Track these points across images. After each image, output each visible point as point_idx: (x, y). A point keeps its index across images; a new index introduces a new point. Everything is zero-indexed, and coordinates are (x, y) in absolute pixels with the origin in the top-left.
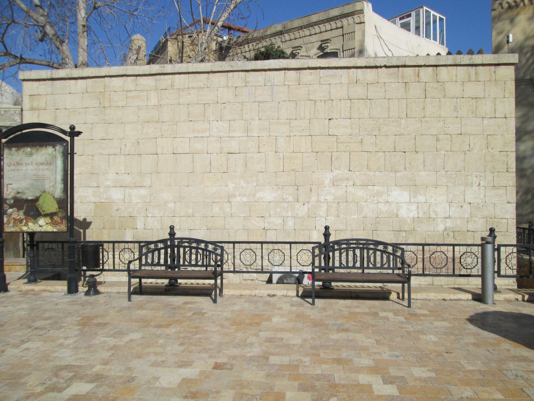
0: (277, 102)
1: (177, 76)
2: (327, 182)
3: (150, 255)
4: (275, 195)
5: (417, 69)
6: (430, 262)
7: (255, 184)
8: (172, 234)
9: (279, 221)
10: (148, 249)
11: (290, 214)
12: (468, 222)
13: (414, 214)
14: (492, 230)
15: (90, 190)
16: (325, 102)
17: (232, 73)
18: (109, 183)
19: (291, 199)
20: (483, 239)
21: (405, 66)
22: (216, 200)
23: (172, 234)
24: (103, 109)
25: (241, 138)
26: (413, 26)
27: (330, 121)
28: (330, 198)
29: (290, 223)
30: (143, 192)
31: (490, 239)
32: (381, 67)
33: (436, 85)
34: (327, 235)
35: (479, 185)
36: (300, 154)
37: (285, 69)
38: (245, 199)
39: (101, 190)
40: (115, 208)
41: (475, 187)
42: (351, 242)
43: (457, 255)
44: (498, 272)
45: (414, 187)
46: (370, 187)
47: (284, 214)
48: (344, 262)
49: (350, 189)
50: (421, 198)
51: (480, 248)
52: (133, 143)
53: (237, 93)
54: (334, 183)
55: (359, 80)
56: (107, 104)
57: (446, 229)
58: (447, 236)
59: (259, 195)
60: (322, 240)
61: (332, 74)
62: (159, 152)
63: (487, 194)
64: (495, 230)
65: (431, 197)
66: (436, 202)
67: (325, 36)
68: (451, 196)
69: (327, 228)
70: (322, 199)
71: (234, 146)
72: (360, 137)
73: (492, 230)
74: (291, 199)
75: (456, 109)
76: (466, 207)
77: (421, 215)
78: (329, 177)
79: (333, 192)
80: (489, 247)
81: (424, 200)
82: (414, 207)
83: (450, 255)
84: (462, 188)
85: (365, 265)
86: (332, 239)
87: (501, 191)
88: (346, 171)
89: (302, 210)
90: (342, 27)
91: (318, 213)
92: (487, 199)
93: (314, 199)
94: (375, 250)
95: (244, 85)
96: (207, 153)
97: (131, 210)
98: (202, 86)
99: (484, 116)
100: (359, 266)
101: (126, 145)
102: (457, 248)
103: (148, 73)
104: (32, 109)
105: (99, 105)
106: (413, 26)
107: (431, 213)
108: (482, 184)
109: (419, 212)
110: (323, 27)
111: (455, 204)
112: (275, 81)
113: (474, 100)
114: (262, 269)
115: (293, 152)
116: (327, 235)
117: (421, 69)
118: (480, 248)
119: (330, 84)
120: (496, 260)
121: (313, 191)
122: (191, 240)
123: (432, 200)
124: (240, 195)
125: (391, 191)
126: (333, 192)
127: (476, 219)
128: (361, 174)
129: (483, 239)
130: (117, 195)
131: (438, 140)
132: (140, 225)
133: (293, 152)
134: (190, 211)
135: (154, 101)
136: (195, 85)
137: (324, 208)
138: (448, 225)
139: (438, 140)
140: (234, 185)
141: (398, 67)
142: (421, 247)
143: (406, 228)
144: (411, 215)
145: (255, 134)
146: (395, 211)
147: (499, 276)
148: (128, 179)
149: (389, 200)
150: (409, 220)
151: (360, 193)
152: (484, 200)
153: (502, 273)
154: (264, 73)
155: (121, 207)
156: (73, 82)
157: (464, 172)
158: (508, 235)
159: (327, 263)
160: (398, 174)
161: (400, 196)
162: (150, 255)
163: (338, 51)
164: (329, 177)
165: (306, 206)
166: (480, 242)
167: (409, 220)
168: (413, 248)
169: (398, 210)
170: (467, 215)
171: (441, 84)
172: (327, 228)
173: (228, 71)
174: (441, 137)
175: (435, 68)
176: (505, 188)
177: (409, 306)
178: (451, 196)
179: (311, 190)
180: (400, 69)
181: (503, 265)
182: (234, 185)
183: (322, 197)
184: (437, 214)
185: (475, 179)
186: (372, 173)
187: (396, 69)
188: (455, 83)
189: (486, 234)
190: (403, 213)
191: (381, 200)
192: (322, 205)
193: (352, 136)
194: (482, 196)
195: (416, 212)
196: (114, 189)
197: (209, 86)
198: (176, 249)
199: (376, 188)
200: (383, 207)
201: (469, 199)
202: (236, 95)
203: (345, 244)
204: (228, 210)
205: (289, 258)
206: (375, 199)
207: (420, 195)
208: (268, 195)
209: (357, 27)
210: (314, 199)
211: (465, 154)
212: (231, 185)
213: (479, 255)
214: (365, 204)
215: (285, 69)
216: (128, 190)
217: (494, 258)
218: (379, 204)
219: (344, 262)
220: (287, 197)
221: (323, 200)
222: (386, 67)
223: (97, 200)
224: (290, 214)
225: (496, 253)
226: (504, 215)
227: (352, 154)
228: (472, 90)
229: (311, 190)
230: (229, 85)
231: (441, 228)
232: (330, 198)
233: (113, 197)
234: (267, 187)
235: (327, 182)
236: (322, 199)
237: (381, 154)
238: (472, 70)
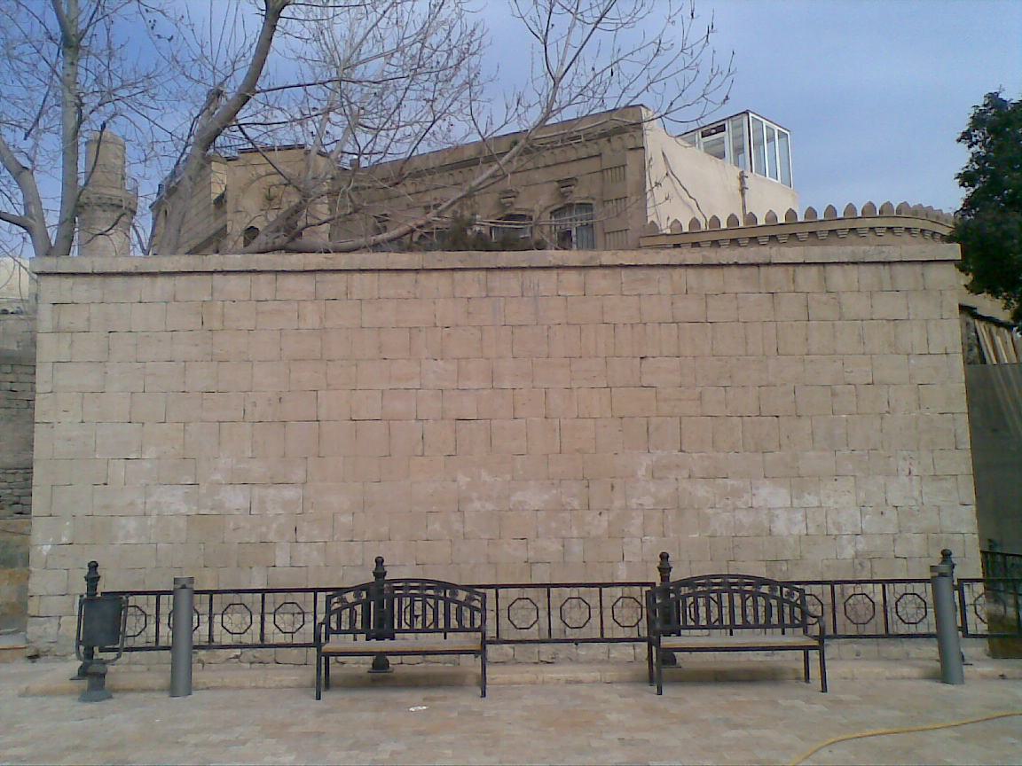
0: (546, 327)
1: (357, 276)
2: (641, 472)
3: (346, 613)
4: (546, 497)
5: (791, 269)
6: (976, 612)
7: (508, 477)
8: (380, 573)
9: (554, 547)
10: (343, 600)
11: (575, 533)
12: (894, 540)
13: (799, 529)
14: (946, 555)
15: (180, 491)
16: (632, 328)
17: (460, 273)
18: (218, 477)
19: (576, 504)
20: (933, 568)
21: (769, 264)
22: (434, 508)
23: (380, 573)
24: (209, 334)
25: (481, 391)
26: (729, 148)
27: (644, 361)
28: (648, 501)
29: (577, 548)
30: (290, 493)
31: (945, 568)
32: (728, 265)
33: (824, 298)
34: (664, 570)
35: (910, 473)
36: (590, 422)
37: (558, 267)
38: (490, 506)
39: (203, 489)
40: (232, 525)
41: (904, 479)
42: (714, 581)
43: (891, 600)
44: (964, 628)
45: (798, 481)
46: (720, 481)
47: (564, 532)
48: (750, 619)
49: (685, 484)
50: (811, 500)
51: (929, 586)
52: (270, 400)
53: (471, 309)
54: (653, 474)
55: (691, 288)
56: (216, 325)
57: (857, 555)
58: (859, 567)
59: (517, 497)
60: (656, 578)
61: (642, 277)
62: (323, 415)
63: (925, 489)
64: (951, 554)
65: (829, 497)
66: (837, 506)
67: (563, 173)
68: (862, 494)
69: (664, 557)
70: (634, 502)
71: (468, 407)
72: (699, 389)
73: (946, 555)
74: (576, 504)
75: (862, 340)
76: (891, 514)
77: (812, 531)
78: (645, 462)
79: (653, 490)
80: (945, 583)
81: (817, 504)
82: (799, 516)
83: (879, 598)
84: (881, 479)
85: (787, 621)
86: (675, 576)
87: (948, 484)
88: (675, 452)
89: (600, 525)
90: (600, 155)
91: (626, 530)
92: (925, 499)
93: (618, 503)
94: (755, 595)
95: (484, 294)
96: (417, 419)
97: (264, 529)
98: (405, 294)
99: (910, 351)
100: (776, 623)
101: (255, 404)
102: (890, 587)
103: (301, 269)
104: (57, 330)
105: (200, 327)
106: (729, 148)
107: (830, 525)
108: (915, 471)
109: (809, 525)
110: (559, 155)
111: (870, 509)
112: (541, 288)
113: (892, 323)
114: (262, 638)
115: (578, 417)
116: (664, 570)
117: (800, 269)
118: (929, 586)
119: (639, 295)
120: (958, 604)
121: (617, 488)
122: (424, 583)
123: (831, 503)
124: (479, 499)
125: (757, 488)
126: (653, 490)
127: (908, 535)
128: (702, 457)
129: (933, 568)
130: (235, 499)
131: (834, 395)
132: (282, 558)
133: (578, 417)
134: (384, 530)
135: (312, 320)
136: (391, 293)
137: (638, 521)
138: (860, 547)
139: (834, 395)
140: (469, 479)
141: (758, 265)
142: (829, 587)
143: (787, 555)
144: (795, 531)
145: (507, 385)
146: (766, 524)
147: (966, 635)
148: (257, 469)
149: (755, 504)
150: (791, 540)
151: (702, 491)
152: (920, 501)
153: (971, 629)
154: (519, 273)
155: (242, 524)
156: (147, 280)
157: (882, 452)
158: (970, 565)
159: (447, 624)
160: (769, 457)
161: (771, 496)
162: (346, 613)
163: (594, 202)
164: (645, 462)
165: (605, 517)
166: (928, 576)
167: (791, 540)
168: (816, 589)
169: (771, 521)
170: (891, 529)
171: (833, 295)
172: (664, 557)
173: (453, 269)
174: (839, 388)
175: (821, 267)
176: (953, 479)
177: (824, 689)
178: (862, 494)
179: (613, 487)
180: (763, 269)
181: (971, 616)
182: (469, 479)
183: (634, 500)
184: (839, 528)
185: (901, 463)
186: (722, 455)
187: (755, 269)
188: (856, 293)
189: (936, 559)
190: (780, 527)
191: (739, 504)
192: (634, 514)
193: (682, 388)
194: (916, 494)
195: (804, 525)
196: (229, 487)
197: (418, 295)
198: (396, 601)
199: (729, 482)
200: (745, 518)
201: (895, 497)
202: (469, 313)
203: (703, 585)
204: (457, 526)
205: (830, 610)
206: (730, 502)
207: (809, 494)
208: (533, 497)
209: (631, 156)
210: (618, 503)
211: (882, 418)
212: (463, 480)
213: (930, 600)
214: (711, 511)
215: (558, 267)
216: (257, 491)
217: (955, 603)
218: (736, 511)
219: (750, 619)
220: (568, 500)
221: (635, 506)
222: (736, 264)
223: (194, 510)
224: (575, 533)
225: (956, 593)
226: (959, 525)
227: (685, 420)
228: (888, 305)
229: (613, 487)
230: (457, 295)
231: (849, 552)
232: (648, 501)
233: (227, 505)
234: (532, 483)
235: (641, 472)
236: (634, 502)
237: (736, 420)
238: (884, 270)
